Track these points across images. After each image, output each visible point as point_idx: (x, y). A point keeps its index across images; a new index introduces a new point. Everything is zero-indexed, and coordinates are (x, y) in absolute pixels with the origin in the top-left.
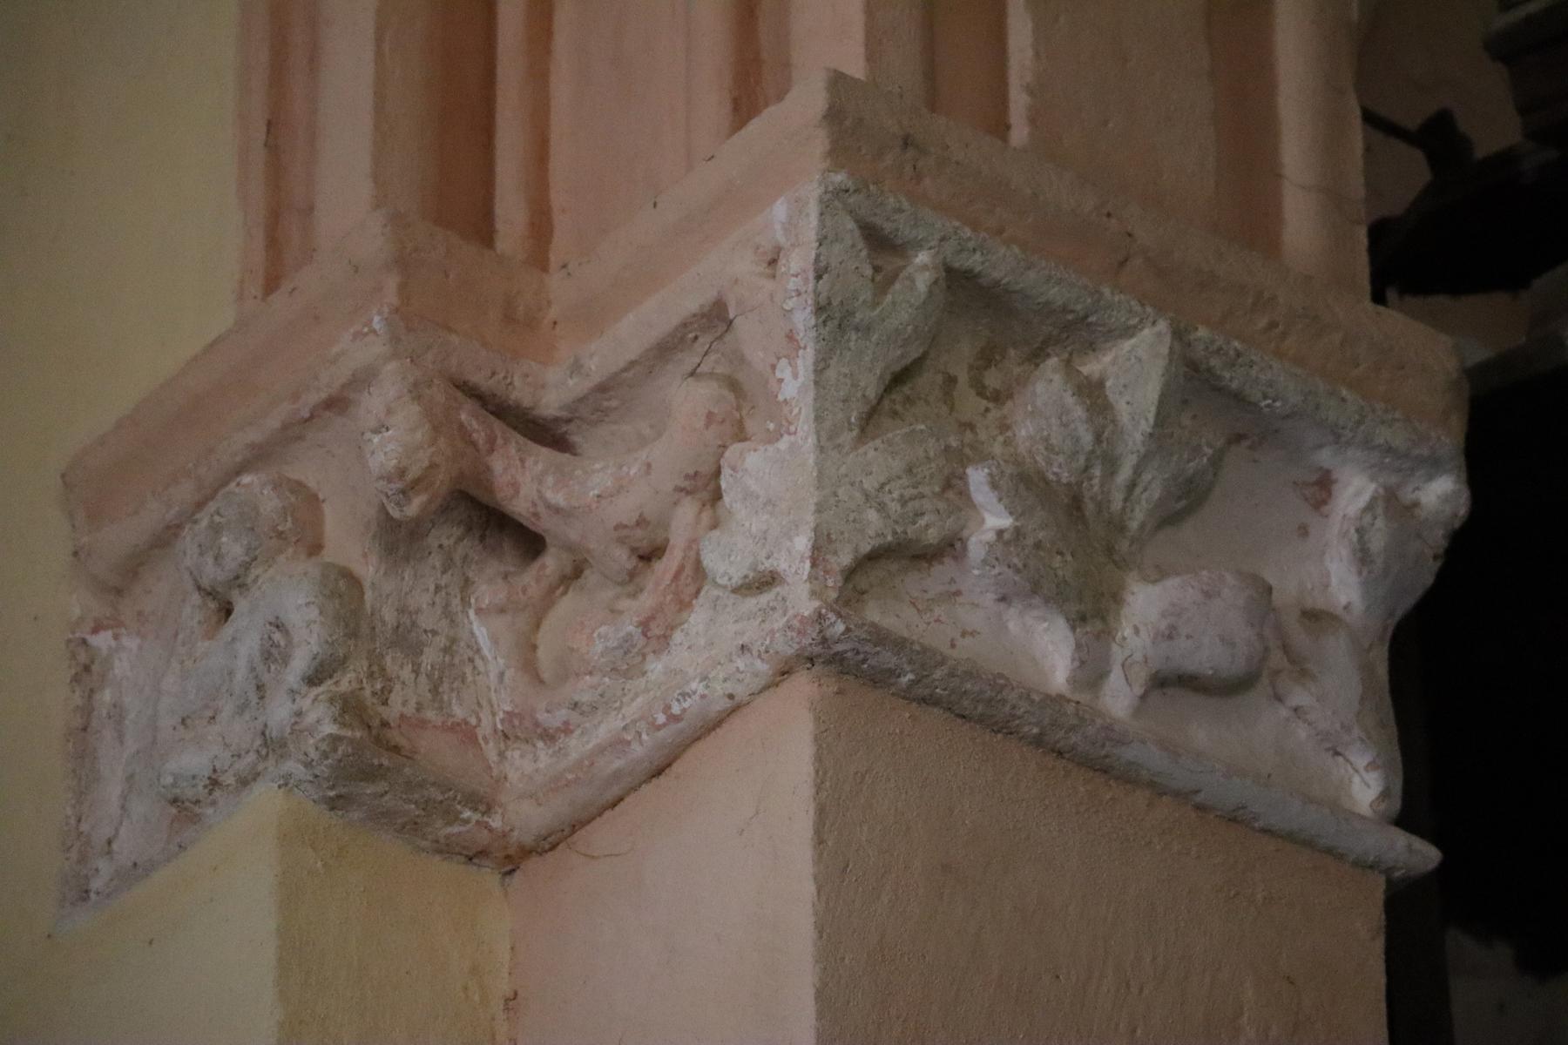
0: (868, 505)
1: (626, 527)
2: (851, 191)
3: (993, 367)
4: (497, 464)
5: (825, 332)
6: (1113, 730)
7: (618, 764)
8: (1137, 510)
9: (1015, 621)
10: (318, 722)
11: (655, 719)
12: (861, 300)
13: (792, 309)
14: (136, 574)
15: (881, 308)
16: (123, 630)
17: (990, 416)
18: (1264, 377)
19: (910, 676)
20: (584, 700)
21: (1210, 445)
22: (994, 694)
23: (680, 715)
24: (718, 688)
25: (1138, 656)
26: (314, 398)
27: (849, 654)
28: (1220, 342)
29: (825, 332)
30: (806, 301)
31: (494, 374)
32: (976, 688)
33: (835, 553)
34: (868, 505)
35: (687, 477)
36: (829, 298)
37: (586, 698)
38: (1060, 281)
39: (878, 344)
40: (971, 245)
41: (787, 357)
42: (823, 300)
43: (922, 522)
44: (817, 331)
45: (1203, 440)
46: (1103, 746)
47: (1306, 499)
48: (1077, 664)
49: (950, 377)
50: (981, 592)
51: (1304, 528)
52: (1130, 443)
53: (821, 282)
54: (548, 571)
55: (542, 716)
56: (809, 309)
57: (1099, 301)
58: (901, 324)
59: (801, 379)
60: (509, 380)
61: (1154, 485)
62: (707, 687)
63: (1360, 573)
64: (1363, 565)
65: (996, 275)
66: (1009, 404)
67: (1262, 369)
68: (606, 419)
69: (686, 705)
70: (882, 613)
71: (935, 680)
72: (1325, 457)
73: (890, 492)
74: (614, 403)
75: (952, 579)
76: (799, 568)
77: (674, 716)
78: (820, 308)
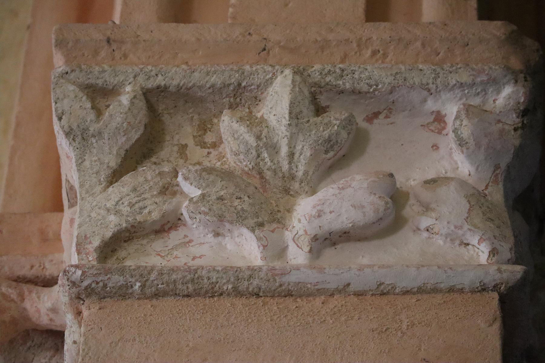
0: (109, 214)
2: (69, 72)
3: (208, 132)
4: (27, 304)
5: (76, 144)
6: (275, 270)
8: (300, 166)
9: (229, 243)
12: (89, 120)
15: (103, 120)
17: (212, 156)
18: (364, 76)
19: (138, 284)
21: (336, 119)
22: (192, 276)
25: (301, 232)
27: (93, 285)
28: (328, 67)
29: (76, 144)
31: (32, 267)
32: (180, 276)
33: (90, 243)
34: (109, 214)
36: (70, 127)
38: (215, 72)
39: (109, 139)
40: (153, 73)
42: (67, 130)
43: (146, 211)
44: (72, 146)
45: (332, 118)
46: (275, 280)
47: (432, 131)
48: (262, 248)
49: (182, 145)
50: (204, 236)
51: (436, 146)
52: (280, 133)
53: (62, 121)
57: (243, 73)
58: (118, 124)
60: (42, 267)
61: (305, 150)
63: (462, 152)
64: (462, 147)
65: (175, 83)
66: (222, 146)
67: (361, 73)
71: (153, 281)
72: (431, 105)
73: (123, 203)
75: (185, 236)
78: (68, 133)
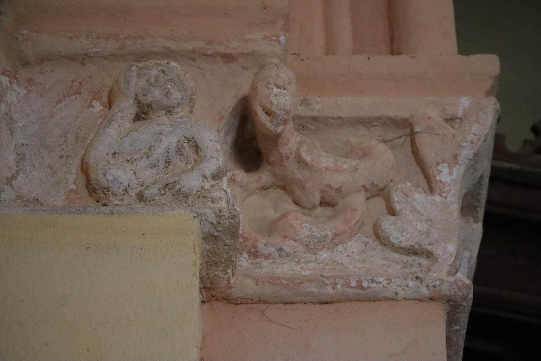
1: (332, 188)
7: (314, 290)
10: (220, 198)
11: (350, 283)
13: (464, 147)
14: (42, 61)
16: (15, 81)
20: (287, 250)
23: (366, 288)
24: (394, 287)
26: (221, 49)
30: (474, 148)
35: (373, 184)
37: (288, 250)
41: (449, 164)
54: (262, 181)
55: (260, 245)
56: (473, 152)
59: (454, 176)
62: (388, 284)
68: (302, 131)
69: (372, 285)
70: (441, 290)
74: (312, 127)
76: (448, 258)
77: (363, 287)
